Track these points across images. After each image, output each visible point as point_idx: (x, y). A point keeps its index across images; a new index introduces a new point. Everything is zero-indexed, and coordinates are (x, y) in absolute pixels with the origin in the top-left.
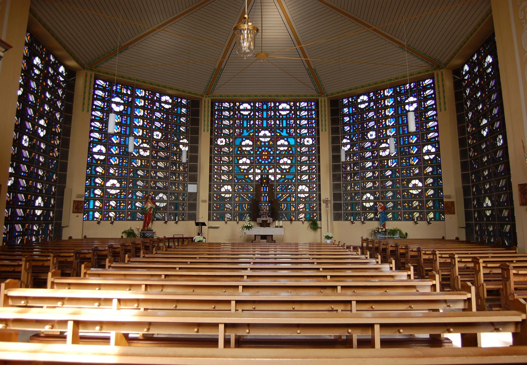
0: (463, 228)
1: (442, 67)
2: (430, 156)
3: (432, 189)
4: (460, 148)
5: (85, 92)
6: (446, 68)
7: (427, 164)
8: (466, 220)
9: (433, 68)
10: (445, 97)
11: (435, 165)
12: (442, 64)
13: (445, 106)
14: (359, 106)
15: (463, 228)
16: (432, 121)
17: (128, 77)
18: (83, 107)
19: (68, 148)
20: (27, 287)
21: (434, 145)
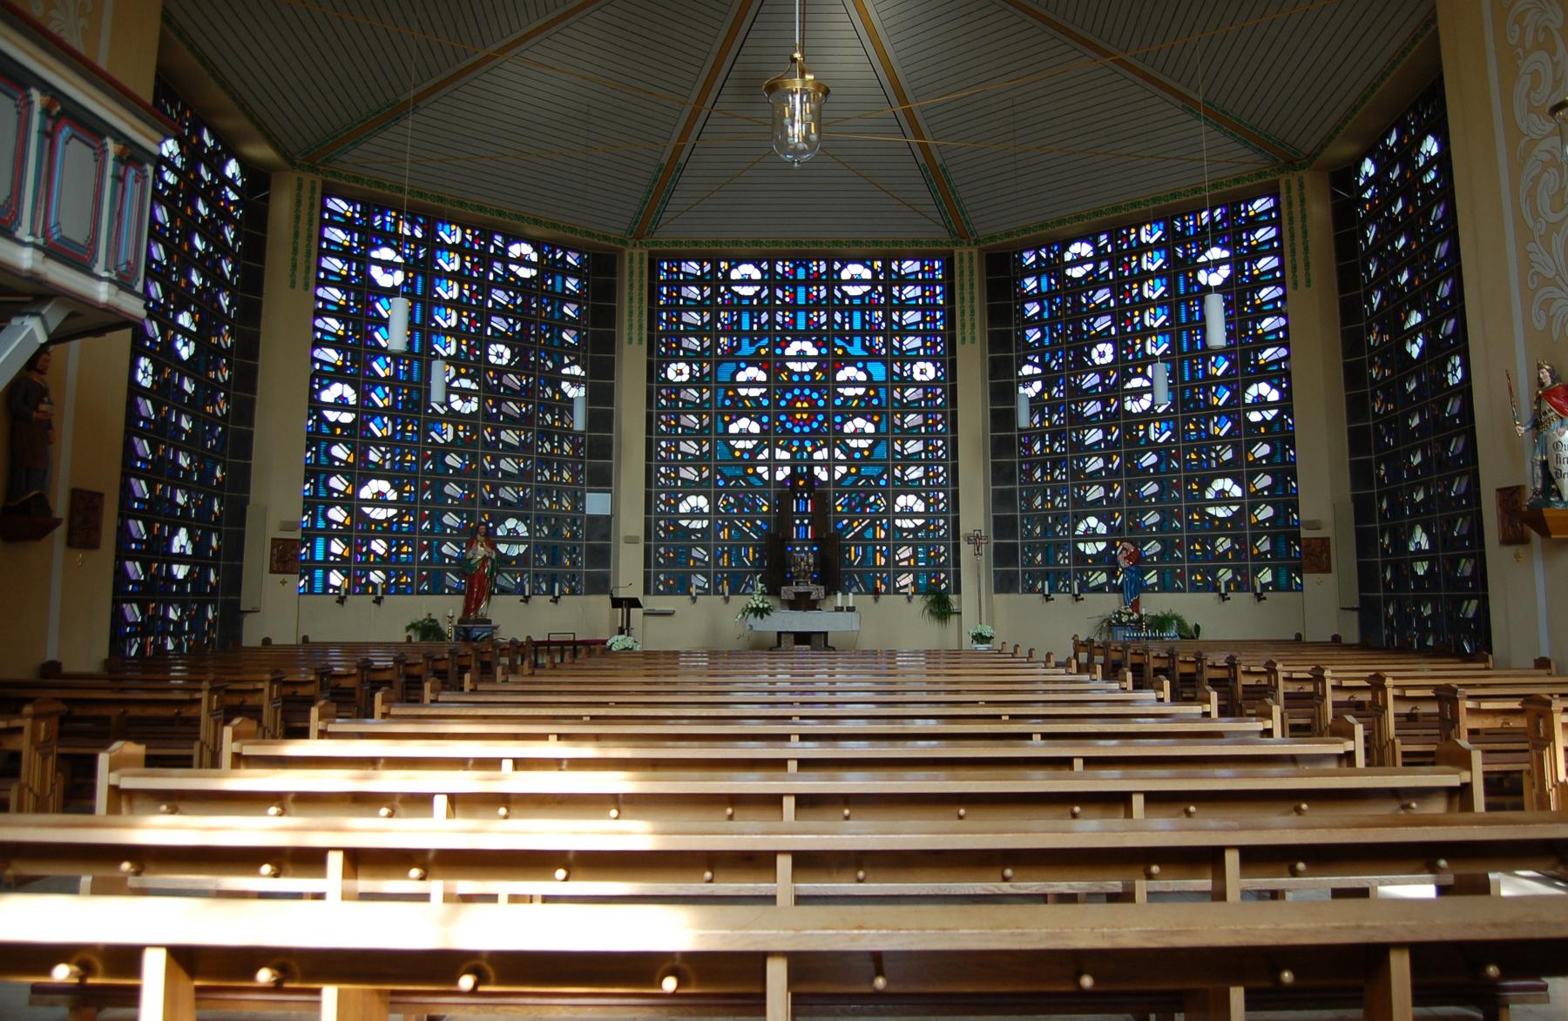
0: (1353, 609)
2: (1264, 413)
5: (296, 234)
15: (1353, 609)
16: (1272, 316)
18: (293, 275)
19: (253, 390)
21: (1276, 382)
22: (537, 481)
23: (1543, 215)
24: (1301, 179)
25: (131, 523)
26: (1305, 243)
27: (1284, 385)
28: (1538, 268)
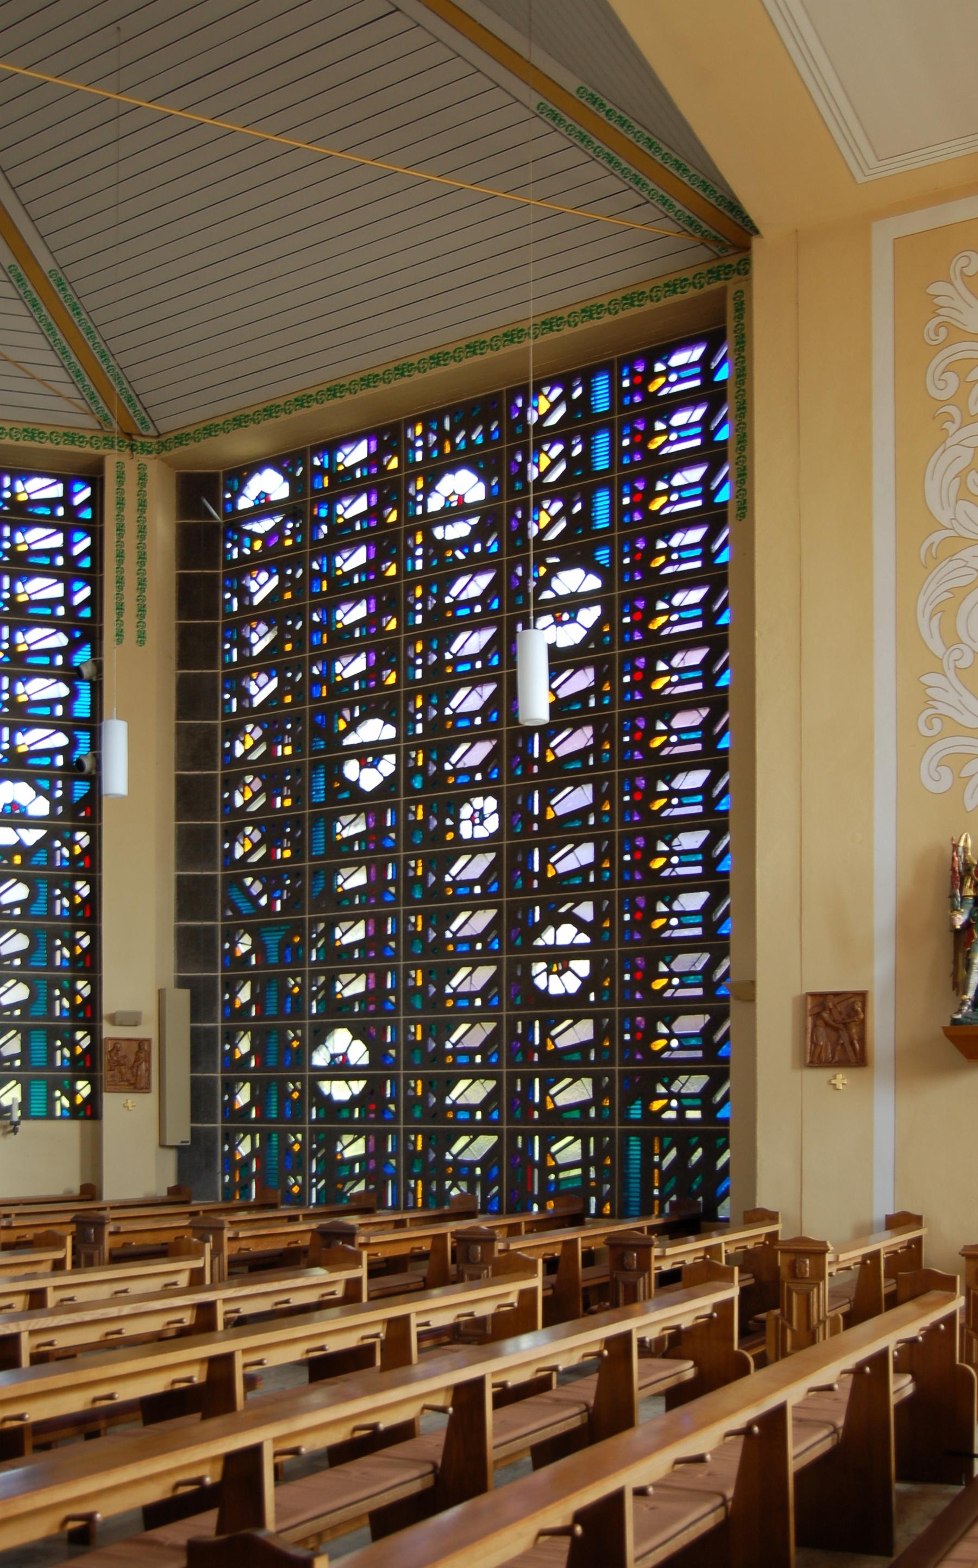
1: (143, 444)
2: (22, 832)
3: (20, 979)
4: (179, 817)
6: (165, 454)
7: (6, 866)
8: (195, 1117)
9: (101, 435)
10: (148, 582)
11: (42, 877)
12: (152, 432)
13: (141, 623)
14: (593, 583)
16: (47, 676)
17: (647, 134)
20: (460, 1367)
21: (45, 784)
22: (302, 1131)
23: (965, 639)
24: (142, 467)
25: (608, 697)
26: (141, 572)
27: (59, 794)
28: (943, 709)
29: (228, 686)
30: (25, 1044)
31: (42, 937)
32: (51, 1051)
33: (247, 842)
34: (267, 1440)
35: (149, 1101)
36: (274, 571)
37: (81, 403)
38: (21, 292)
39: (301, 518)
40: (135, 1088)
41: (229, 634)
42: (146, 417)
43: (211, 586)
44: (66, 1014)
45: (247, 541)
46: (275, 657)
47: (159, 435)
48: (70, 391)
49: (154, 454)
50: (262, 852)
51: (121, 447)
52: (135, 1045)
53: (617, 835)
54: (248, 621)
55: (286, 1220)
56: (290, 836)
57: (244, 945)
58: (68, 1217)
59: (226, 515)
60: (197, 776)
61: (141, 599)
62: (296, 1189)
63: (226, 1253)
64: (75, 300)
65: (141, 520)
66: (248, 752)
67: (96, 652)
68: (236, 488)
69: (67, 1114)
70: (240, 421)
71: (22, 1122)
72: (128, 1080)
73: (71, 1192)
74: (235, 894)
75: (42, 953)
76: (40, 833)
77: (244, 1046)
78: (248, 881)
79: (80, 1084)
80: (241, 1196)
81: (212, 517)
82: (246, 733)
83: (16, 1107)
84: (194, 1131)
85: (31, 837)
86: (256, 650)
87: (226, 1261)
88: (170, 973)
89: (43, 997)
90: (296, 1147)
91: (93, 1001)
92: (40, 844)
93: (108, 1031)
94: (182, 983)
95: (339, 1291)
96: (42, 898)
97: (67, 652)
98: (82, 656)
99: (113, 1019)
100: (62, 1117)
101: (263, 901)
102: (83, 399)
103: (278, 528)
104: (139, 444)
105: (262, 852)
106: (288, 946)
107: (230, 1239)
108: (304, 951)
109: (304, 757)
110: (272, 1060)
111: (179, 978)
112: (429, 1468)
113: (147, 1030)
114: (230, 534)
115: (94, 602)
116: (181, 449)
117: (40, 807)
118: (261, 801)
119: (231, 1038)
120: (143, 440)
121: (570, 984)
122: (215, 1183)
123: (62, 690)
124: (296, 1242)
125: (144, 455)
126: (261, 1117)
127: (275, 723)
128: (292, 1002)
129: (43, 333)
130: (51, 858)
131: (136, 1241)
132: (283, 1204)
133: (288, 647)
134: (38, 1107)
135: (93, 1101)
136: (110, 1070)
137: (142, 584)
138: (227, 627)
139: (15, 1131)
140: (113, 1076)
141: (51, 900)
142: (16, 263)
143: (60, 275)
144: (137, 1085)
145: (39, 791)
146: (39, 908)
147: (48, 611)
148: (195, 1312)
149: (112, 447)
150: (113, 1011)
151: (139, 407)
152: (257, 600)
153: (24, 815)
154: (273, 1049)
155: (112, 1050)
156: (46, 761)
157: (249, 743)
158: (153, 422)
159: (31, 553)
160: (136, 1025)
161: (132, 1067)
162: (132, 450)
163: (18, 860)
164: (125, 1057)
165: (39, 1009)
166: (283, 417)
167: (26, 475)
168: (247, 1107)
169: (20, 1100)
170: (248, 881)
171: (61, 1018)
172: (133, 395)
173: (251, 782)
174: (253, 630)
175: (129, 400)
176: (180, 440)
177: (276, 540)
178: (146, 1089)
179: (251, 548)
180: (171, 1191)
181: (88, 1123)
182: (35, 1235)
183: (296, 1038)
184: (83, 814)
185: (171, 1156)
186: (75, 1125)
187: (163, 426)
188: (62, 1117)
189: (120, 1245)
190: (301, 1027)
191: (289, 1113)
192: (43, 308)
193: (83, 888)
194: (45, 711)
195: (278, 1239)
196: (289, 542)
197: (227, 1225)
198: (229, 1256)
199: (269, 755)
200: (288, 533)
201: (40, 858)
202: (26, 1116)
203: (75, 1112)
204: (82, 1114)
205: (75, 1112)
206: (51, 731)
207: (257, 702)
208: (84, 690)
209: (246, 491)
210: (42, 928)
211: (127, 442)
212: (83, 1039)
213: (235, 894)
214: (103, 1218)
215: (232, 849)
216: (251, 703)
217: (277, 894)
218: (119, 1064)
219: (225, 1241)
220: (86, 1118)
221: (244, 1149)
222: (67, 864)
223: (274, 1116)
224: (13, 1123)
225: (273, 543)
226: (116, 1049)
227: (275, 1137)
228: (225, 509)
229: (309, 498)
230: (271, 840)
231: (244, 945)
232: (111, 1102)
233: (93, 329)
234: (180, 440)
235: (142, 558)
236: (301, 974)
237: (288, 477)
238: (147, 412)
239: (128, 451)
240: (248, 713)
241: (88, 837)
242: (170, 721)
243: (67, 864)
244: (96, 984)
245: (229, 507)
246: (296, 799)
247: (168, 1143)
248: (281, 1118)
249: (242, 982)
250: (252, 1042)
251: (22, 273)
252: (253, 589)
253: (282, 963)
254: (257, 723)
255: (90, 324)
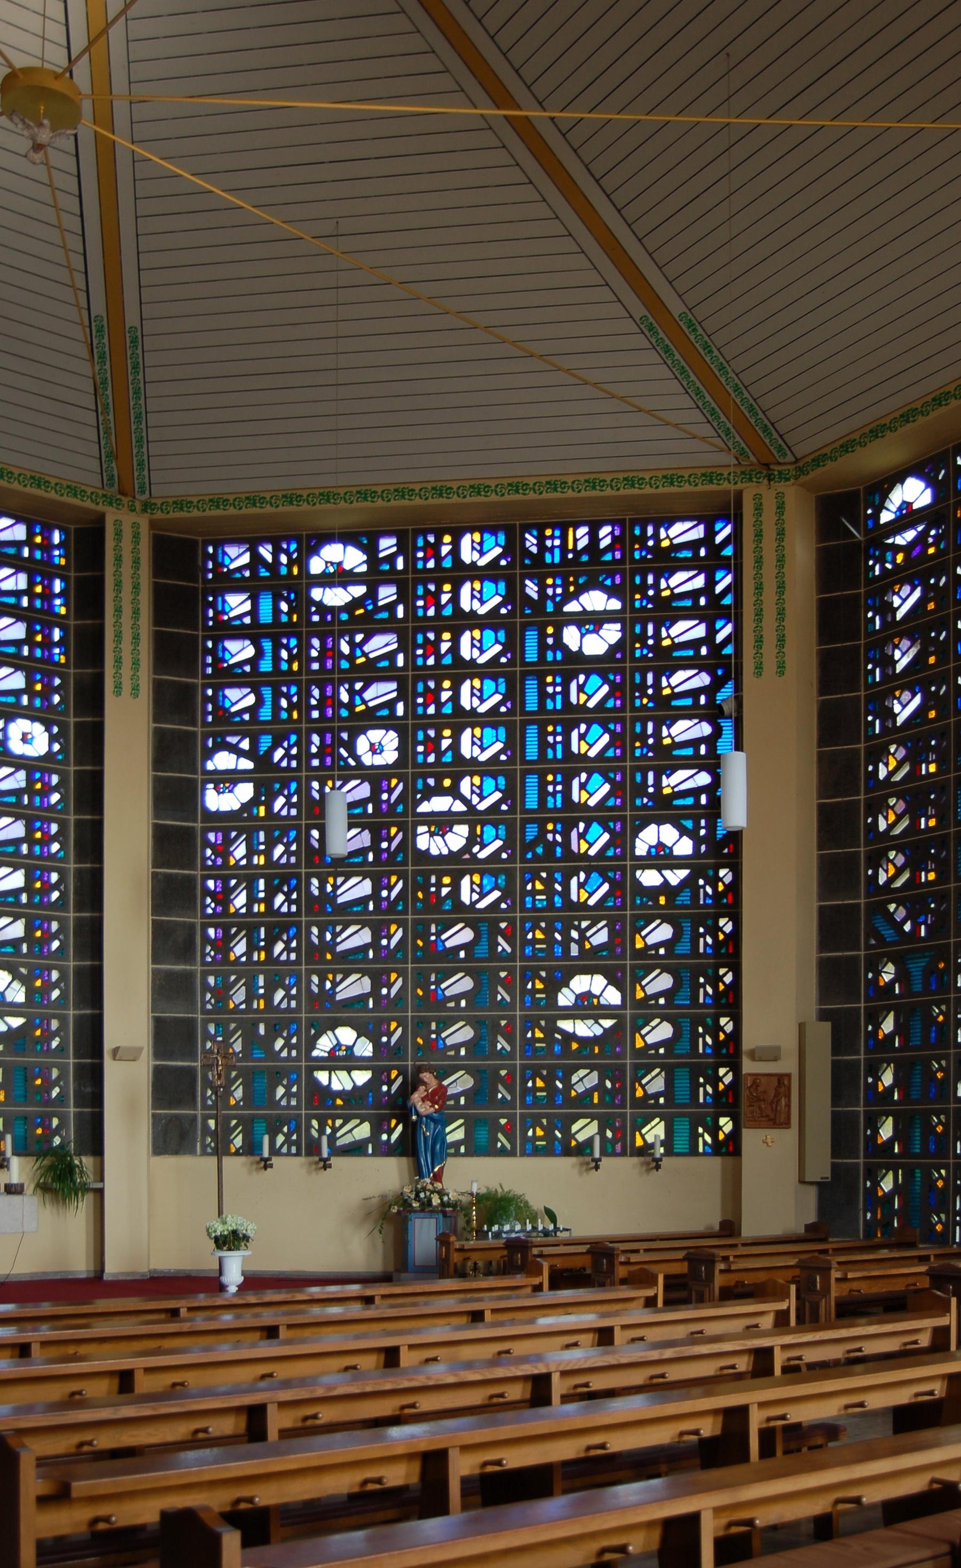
1: (780, 473)
2: (667, 873)
3: (664, 1018)
4: (821, 847)
6: (803, 479)
8: (835, 1153)
12: (790, 458)
16: (690, 717)
21: (689, 824)
22: (946, 1167)
24: (780, 496)
26: (780, 601)
29: (870, 708)
30: (669, 1082)
31: (686, 975)
32: (695, 1086)
33: (891, 867)
34: (705, 1509)
35: (788, 1137)
36: (916, 583)
37: (718, 441)
38: (653, 341)
39: (943, 523)
40: (775, 1123)
41: (871, 654)
42: (783, 444)
43: (853, 607)
44: (709, 1051)
45: (889, 556)
46: (918, 672)
47: (797, 461)
48: (707, 430)
49: (792, 481)
50: (906, 876)
51: (759, 478)
52: (775, 1080)
53: (862, 793)
54: (890, 638)
55: (916, 1261)
56: (934, 858)
57: (888, 973)
58: (680, 1255)
59: (867, 532)
60: (839, 803)
61: (780, 629)
62: (939, 1228)
63: (834, 1294)
64: (706, 338)
65: (780, 548)
66: (891, 774)
67: (738, 688)
68: (877, 502)
69: (709, 1150)
70: (876, 432)
71: (664, 1159)
72: (767, 1116)
73: (712, 1228)
74: (880, 923)
75: (686, 991)
76: (683, 873)
77: (887, 1078)
78: (892, 907)
79: (722, 1121)
80: (882, 1234)
81: (853, 536)
82: (889, 753)
83: (658, 1144)
84: (834, 1167)
85: (675, 877)
86: (899, 667)
87: (833, 1303)
88: (812, 1006)
89: (686, 1036)
90: (940, 1184)
91: (735, 1037)
92: (684, 883)
93: (748, 1066)
94: (823, 1016)
95: (924, 1340)
96: (686, 937)
97: (710, 691)
98: (726, 693)
99: (753, 1055)
100: (705, 1154)
101: (907, 927)
102: (719, 436)
103: (920, 540)
104: (776, 473)
105: (906, 876)
106: (932, 973)
107: (837, 1280)
108: (949, 978)
109: (949, 773)
110: (915, 1094)
111: (821, 1010)
112: (945, 1548)
113: (788, 1065)
114: (871, 551)
115: (736, 638)
116: (820, 470)
117: (685, 847)
118: (905, 823)
119: (874, 1071)
120: (780, 468)
121: (580, 983)
122: (857, 1220)
123: (706, 729)
124: (915, 1285)
125: (782, 483)
126: (905, 1152)
127: (919, 740)
128: (936, 1032)
129: (676, 378)
130: (695, 896)
131: (748, 1279)
132: (923, 1242)
133: (932, 660)
134: (681, 1144)
135: (735, 1136)
136: (750, 1106)
137: (781, 613)
138: (869, 648)
139: (658, 1167)
140: (752, 1112)
141: (696, 937)
142: (647, 314)
143: (690, 316)
144: (777, 1120)
145: (683, 831)
146: (683, 947)
147: (691, 653)
148: (752, 1358)
149: (750, 480)
150: (752, 1047)
151: (775, 435)
152: (899, 615)
153: (670, 855)
154: (917, 1080)
155: (752, 1086)
156: (689, 801)
157: (893, 764)
158: (789, 448)
159: (674, 597)
160: (776, 1060)
161: (772, 1102)
162: (769, 480)
163: (662, 900)
164: (764, 1092)
165: (683, 1047)
166: (921, 420)
167: (670, 523)
168: (890, 1142)
169: (662, 1137)
170: (892, 907)
171: (705, 1055)
172: (768, 424)
173: (895, 805)
174: (896, 647)
175: (765, 428)
176: (818, 461)
177: (918, 549)
178: (786, 1124)
179: (893, 562)
180: (809, 1228)
181: (730, 1160)
182: (630, 1272)
183: (941, 1069)
184: (726, 851)
185: (812, 1192)
186: (717, 1162)
187: (800, 451)
188: (705, 1154)
189: (733, 1283)
190: (946, 1057)
191: (932, 1147)
192: (676, 353)
193: (726, 925)
194: (689, 751)
195: (894, 1281)
196: (931, 551)
197: (834, 1265)
198: (836, 1298)
199: (914, 774)
200: (930, 540)
201: (684, 898)
202: (669, 1152)
203: (717, 1148)
204: (724, 1150)
205: (717, 1148)
206: (693, 771)
207: (900, 720)
208: (727, 727)
209: (888, 504)
210: (686, 966)
211: (765, 472)
212: (726, 1076)
213: (880, 923)
214: (713, 1255)
215: (876, 875)
216: (895, 722)
217: (921, 919)
218: (759, 1099)
219: (833, 1281)
220: (728, 1154)
221: (887, 1185)
222: (710, 901)
223: (918, 1151)
224: (595, 1160)
225: (914, 553)
226: (755, 1085)
227: (918, 1173)
228: (866, 525)
229: (952, 501)
230: (915, 864)
231: (888, 973)
232: (751, 1138)
233: (726, 365)
234: (818, 461)
235: (781, 587)
236: (946, 1001)
237: (930, 482)
238: (783, 440)
239: (766, 481)
240: (893, 733)
241: (730, 873)
242: (812, 749)
243: (710, 901)
244: (737, 1020)
245: (870, 523)
246: (940, 819)
247: (807, 1180)
248: (925, 1153)
249: (885, 1013)
250: (895, 1075)
251: (654, 322)
252: (896, 605)
253: (926, 991)
254: (900, 743)
255: (722, 360)
